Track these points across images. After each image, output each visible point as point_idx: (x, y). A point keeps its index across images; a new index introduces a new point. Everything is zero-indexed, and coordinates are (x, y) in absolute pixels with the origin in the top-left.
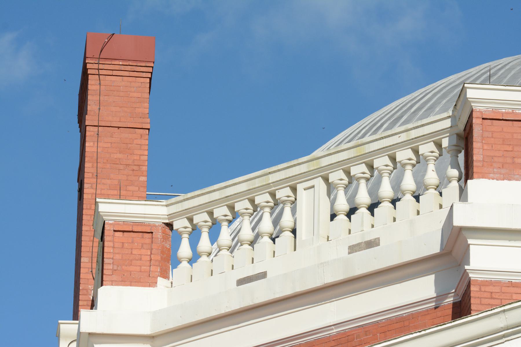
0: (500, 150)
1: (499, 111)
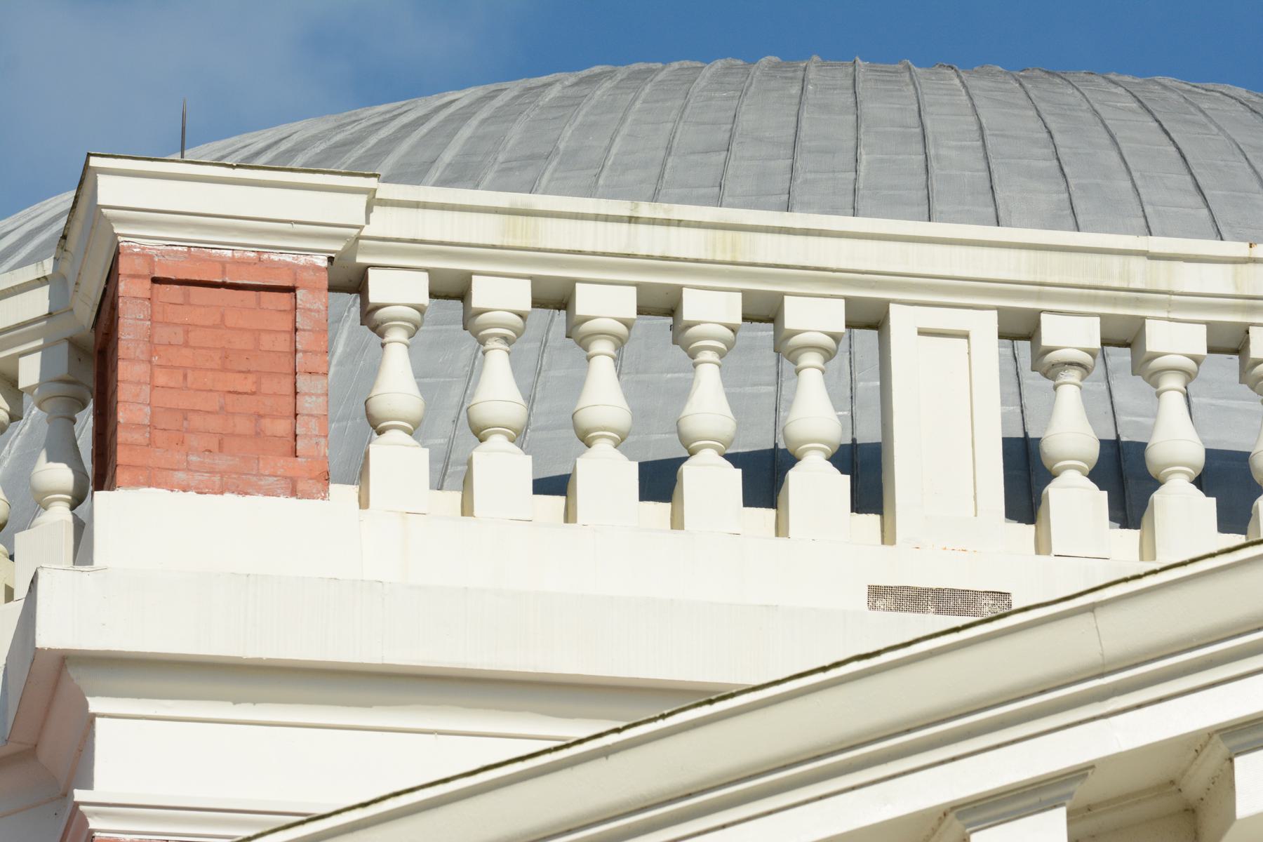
0: (211, 390)
1: (210, 255)
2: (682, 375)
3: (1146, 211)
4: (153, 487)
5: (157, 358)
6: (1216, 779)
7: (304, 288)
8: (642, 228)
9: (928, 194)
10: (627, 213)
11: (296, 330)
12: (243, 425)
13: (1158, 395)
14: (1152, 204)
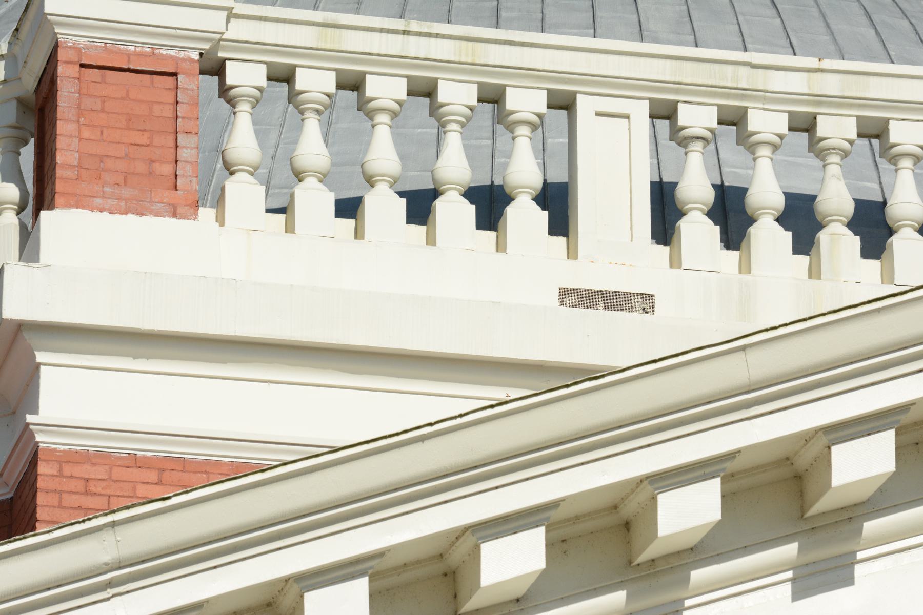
0: (119, 143)
1: (120, 49)
2: (428, 130)
3: (739, 19)
4: (80, 208)
5: (83, 119)
6: (818, 459)
7: (183, 74)
8: (412, 39)
9: (593, 4)
10: (402, 28)
11: (177, 103)
12: (141, 167)
13: (755, 160)
14: (743, 14)
